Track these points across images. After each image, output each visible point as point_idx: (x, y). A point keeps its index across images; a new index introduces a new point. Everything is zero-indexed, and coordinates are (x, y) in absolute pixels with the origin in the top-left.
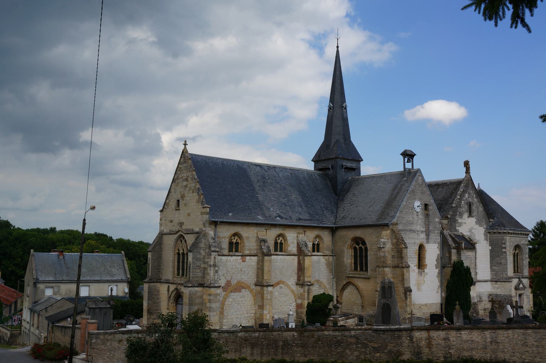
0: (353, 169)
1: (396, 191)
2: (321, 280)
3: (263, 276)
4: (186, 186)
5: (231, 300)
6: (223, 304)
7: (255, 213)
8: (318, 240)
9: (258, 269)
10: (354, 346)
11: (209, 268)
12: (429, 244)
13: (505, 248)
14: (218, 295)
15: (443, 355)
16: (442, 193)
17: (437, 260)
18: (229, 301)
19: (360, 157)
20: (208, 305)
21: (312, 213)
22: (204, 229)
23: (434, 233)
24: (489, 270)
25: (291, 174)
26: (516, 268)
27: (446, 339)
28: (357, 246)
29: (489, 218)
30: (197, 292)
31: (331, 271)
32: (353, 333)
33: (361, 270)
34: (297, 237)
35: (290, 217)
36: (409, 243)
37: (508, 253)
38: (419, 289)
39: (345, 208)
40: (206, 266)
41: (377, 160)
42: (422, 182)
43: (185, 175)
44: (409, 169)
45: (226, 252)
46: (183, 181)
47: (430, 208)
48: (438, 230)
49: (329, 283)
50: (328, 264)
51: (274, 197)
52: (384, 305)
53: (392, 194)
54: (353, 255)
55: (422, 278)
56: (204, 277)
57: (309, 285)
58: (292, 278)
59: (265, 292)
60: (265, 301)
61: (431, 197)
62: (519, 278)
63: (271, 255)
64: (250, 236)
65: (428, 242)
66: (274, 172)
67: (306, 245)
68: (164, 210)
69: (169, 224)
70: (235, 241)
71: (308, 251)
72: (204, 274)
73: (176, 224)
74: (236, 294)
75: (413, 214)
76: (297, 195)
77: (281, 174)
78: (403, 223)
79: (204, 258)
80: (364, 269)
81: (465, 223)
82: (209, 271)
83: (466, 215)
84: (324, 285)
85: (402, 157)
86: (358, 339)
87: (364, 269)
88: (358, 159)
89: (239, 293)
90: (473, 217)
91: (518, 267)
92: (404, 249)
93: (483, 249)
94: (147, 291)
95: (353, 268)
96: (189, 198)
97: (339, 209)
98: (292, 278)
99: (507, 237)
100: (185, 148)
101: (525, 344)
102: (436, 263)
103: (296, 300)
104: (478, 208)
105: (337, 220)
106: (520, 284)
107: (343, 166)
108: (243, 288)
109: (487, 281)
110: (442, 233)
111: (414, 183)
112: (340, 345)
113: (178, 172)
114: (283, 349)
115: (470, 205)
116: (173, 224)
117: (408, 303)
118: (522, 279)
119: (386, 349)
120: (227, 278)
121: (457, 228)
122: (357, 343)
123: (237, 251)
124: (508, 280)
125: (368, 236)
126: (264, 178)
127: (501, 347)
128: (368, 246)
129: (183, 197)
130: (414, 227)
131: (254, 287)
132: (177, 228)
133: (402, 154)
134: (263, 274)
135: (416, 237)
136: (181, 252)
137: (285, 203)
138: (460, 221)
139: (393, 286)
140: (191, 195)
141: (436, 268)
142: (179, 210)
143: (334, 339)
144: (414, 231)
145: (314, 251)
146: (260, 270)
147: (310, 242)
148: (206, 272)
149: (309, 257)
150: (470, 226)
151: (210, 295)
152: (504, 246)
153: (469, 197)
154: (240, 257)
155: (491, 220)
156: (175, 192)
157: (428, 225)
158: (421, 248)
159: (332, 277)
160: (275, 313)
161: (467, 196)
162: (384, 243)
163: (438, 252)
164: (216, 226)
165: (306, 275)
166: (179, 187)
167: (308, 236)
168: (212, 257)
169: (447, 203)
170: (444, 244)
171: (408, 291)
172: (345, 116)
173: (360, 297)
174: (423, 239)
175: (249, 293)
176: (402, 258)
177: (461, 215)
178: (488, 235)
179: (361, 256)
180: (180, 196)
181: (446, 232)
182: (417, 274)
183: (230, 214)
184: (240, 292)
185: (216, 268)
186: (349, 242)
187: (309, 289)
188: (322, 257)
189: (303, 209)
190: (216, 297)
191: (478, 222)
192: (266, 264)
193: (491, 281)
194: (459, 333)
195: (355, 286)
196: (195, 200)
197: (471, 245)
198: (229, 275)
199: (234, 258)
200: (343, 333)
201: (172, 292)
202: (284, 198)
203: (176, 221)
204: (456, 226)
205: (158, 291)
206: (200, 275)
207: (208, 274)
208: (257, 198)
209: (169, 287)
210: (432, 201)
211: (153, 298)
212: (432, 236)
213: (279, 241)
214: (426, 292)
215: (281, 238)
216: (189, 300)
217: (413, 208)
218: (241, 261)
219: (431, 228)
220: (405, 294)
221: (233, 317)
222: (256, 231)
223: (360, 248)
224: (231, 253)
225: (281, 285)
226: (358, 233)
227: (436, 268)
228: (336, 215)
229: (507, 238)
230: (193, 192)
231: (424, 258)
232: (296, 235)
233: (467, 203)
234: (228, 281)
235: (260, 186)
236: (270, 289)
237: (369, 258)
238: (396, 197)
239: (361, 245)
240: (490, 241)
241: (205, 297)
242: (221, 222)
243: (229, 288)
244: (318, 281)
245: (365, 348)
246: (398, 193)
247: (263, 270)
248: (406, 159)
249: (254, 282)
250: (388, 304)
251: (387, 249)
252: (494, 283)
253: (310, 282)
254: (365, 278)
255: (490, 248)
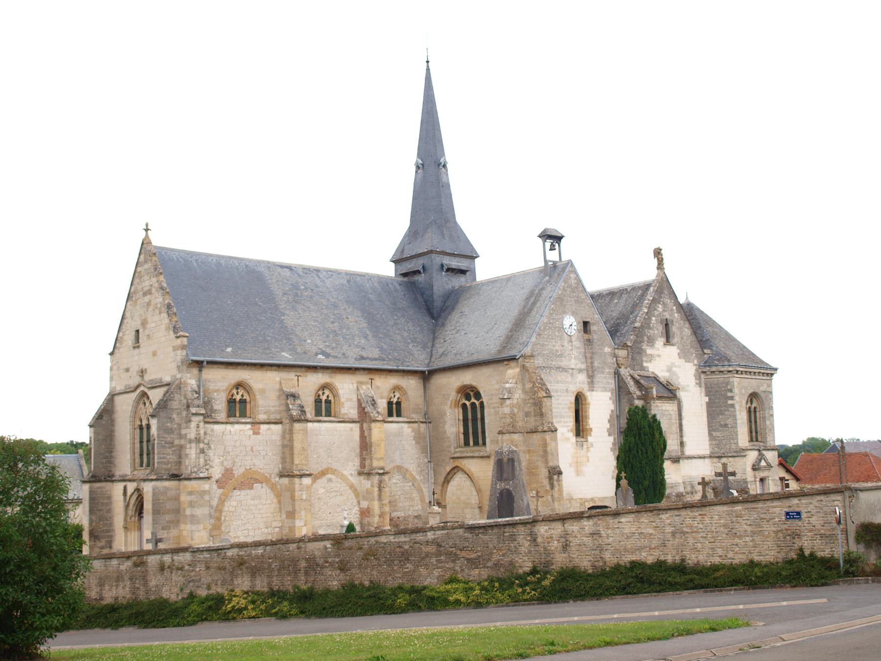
0: (463, 272)
1: (532, 300)
2: (406, 466)
3: (292, 459)
4: (149, 304)
5: (234, 503)
6: (219, 510)
7: (276, 347)
8: (397, 395)
9: (284, 446)
10: (434, 560)
11: (188, 446)
12: (594, 393)
13: (732, 398)
14: (208, 492)
15: (590, 564)
16: (617, 308)
17: (609, 421)
18: (230, 505)
19: (476, 253)
20: (188, 512)
21: (385, 347)
22: (179, 376)
23: (603, 373)
24: (707, 438)
25: (349, 281)
26: (754, 434)
27: (595, 534)
28: (468, 403)
29: (702, 348)
30: (167, 489)
31: (423, 450)
32: (430, 535)
33: (476, 443)
34: (358, 389)
35: (344, 354)
36: (557, 391)
37: (737, 407)
38: (578, 473)
39: (447, 338)
40: (183, 442)
41: (501, 251)
42: (577, 284)
43: (147, 283)
44: (555, 263)
45: (222, 416)
46: (145, 294)
47: (593, 328)
48: (610, 368)
49: (421, 471)
50: (418, 438)
51: (315, 321)
52: (501, 493)
53: (525, 307)
54: (461, 418)
55: (583, 452)
56: (180, 463)
57: (380, 474)
58: (351, 464)
59: (297, 487)
60: (297, 504)
61: (594, 310)
62: (759, 451)
63: (308, 421)
64: (265, 386)
65: (592, 389)
66: (317, 278)
67: (374, 403)
68: (116, 351)
69: (125, 375)
70: (238, 398)
71: (378, 412)
72: (180, 457)
73: (135, 374)
74: (243, 492)
75: (561, 339)
76: (358, 317)
77: (328, 282)
78: (544, 355)
79: (180, 429)
80: (480, 441)
81: (659, 356)
82: (188, 451)
83: (660, 342)
84: (411, 475)
85: (540, 240)
86: (441, 546)
87: (480, 441)
88: (472, 257)
89: (248, 491)
90: (673, 345)
91: (756, 432)
92: (545, 399)
93: (694, 401)
94: (151, 499)
95: (462, 441)
96: (153, 325)
97: (437, 341)
98: (351, 464)
99: (735, 379)
100: (147, 235)
101: (732, 533)
102: (608, 426)
103: (359, 503)
104: (682, 330)
105: (433, 360)
106: (760, 461)
107: (442, 266)
108: (257, 481)
109: (704, 458)
110: (617, 374)
111: (561, 284)
112: (407, 559)
113: (137, 281)
114: (306, 573)
115: (667, 325)
116: (129, 374)
117: (556, 495)
118: (764, 452)
119: (489, 560)
120: (225, 463)
121: (645, 364)
122: (439, 554)
123: (243, 414)
124: (740, 453)
125: (484, 381)
126: (297, 288)
127: (691, 541)
128: (485, 399)
129: (144, 323)
130: (564, 363)
131: (277, 479)
132: (136, 380)
133: (540, 236)
134: (292, 455)
135: (569, 379)
136: (144, 423)
137: (335, 331)
138: (649, 351)
139: (516, 459)
140: (156, 318)
141: (610, 435)
142: (138, 347)
143: (398, 550)
144: (564, 370)
145: (390, 414)
146: (287, 447)
147: (382, 398)
148: (183, 453)
149: (378, 424)
150: (667, 361)
151: (190, 493)
152: (729, 394)
153: (664, 311)
154: (249, 426)
155: (706, 351)
156: (132, 317)
157: (591, 358)
158: (579, 400)
159: (426, 460)
160: (320, 527)
161: (660, 308)
162: (510, 391)
163: (612, 407)
164: (200, 371)
165: (375, 456)
166: (138, 307)
167: (378, 387)
168: (193, 425)
169: (626, 322)
170: (621, 390)
171: (555, 473)
172: (444, 180)
173: (475, 493)
174: (583, 383)
175: (269, 491)
176: (542, 415)
177: (651, 342)
178: (703, 376)
179: (474, 419)
180: (139, 323)
181: (623, 371)
182: (575, 446)
183: (229, 350)
184: (251, 488)
185: (202, 445)
186: (453, 396)
187: (381, 482)
188: (406, 425)
189: (368, 340)
190: (202, 497)
191: (684, 355)
192: (298, 438)
193: (710, 457)
194: (616, 521)
195: (466, 473)
196: (163, 327)
197: (670, 392)
198: (229, 458)
199: (237, 427)
200: (413, 536)
201: (131, 496)
202: (333, 323)
203: (135, 369)
204: (642, 361)
205: (109, 498)
206: (173, 458)
207: (187, 455)
208: (282, 322)
209: (125, 487)
210: (597, 316)
211: (100, 510)
212: (599, 378)
213: (324, 398)
214: (589, 471)
215: (327, 392)
216: (153, 505)
217: (561, 328)
218: (251, 432)
219: (596, 364)
220: (550, 478)
221: (240, 534)
222: (278, 379)
223: (473, 404)
224: (232, 419)
225: (330, 476)
226: (467, 378)
227: (610, 435)
228: (432, 351)
229: (736, 380)
230: (160, 313)
231: (587, 417)
232: (355, 385)
233: (661, 322)
234: (227, 470)
235: (288, 301)
236: (306, 481)
237: (486, 421)
238: (531, 310)
239: (473, 400)
240: (706, 388)
241: (184, 498)
242: (209, 363)
243: (228, 482)
244: (399, 468)
245: (453, 561)
246: (534, 303)
247: (292, 448)
248: (548, 244)
249: (276, 471)
250: (508, 490)
251: (515, 402)
252: (715, 460)
253: (382, 468)
254: (482, 457)
255: (707, 399)
